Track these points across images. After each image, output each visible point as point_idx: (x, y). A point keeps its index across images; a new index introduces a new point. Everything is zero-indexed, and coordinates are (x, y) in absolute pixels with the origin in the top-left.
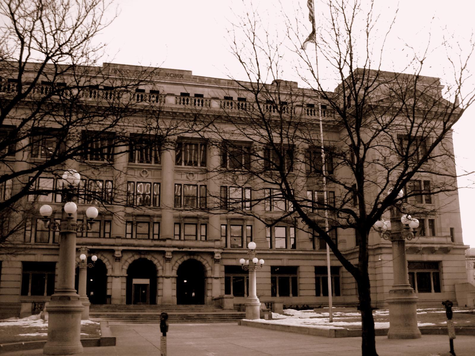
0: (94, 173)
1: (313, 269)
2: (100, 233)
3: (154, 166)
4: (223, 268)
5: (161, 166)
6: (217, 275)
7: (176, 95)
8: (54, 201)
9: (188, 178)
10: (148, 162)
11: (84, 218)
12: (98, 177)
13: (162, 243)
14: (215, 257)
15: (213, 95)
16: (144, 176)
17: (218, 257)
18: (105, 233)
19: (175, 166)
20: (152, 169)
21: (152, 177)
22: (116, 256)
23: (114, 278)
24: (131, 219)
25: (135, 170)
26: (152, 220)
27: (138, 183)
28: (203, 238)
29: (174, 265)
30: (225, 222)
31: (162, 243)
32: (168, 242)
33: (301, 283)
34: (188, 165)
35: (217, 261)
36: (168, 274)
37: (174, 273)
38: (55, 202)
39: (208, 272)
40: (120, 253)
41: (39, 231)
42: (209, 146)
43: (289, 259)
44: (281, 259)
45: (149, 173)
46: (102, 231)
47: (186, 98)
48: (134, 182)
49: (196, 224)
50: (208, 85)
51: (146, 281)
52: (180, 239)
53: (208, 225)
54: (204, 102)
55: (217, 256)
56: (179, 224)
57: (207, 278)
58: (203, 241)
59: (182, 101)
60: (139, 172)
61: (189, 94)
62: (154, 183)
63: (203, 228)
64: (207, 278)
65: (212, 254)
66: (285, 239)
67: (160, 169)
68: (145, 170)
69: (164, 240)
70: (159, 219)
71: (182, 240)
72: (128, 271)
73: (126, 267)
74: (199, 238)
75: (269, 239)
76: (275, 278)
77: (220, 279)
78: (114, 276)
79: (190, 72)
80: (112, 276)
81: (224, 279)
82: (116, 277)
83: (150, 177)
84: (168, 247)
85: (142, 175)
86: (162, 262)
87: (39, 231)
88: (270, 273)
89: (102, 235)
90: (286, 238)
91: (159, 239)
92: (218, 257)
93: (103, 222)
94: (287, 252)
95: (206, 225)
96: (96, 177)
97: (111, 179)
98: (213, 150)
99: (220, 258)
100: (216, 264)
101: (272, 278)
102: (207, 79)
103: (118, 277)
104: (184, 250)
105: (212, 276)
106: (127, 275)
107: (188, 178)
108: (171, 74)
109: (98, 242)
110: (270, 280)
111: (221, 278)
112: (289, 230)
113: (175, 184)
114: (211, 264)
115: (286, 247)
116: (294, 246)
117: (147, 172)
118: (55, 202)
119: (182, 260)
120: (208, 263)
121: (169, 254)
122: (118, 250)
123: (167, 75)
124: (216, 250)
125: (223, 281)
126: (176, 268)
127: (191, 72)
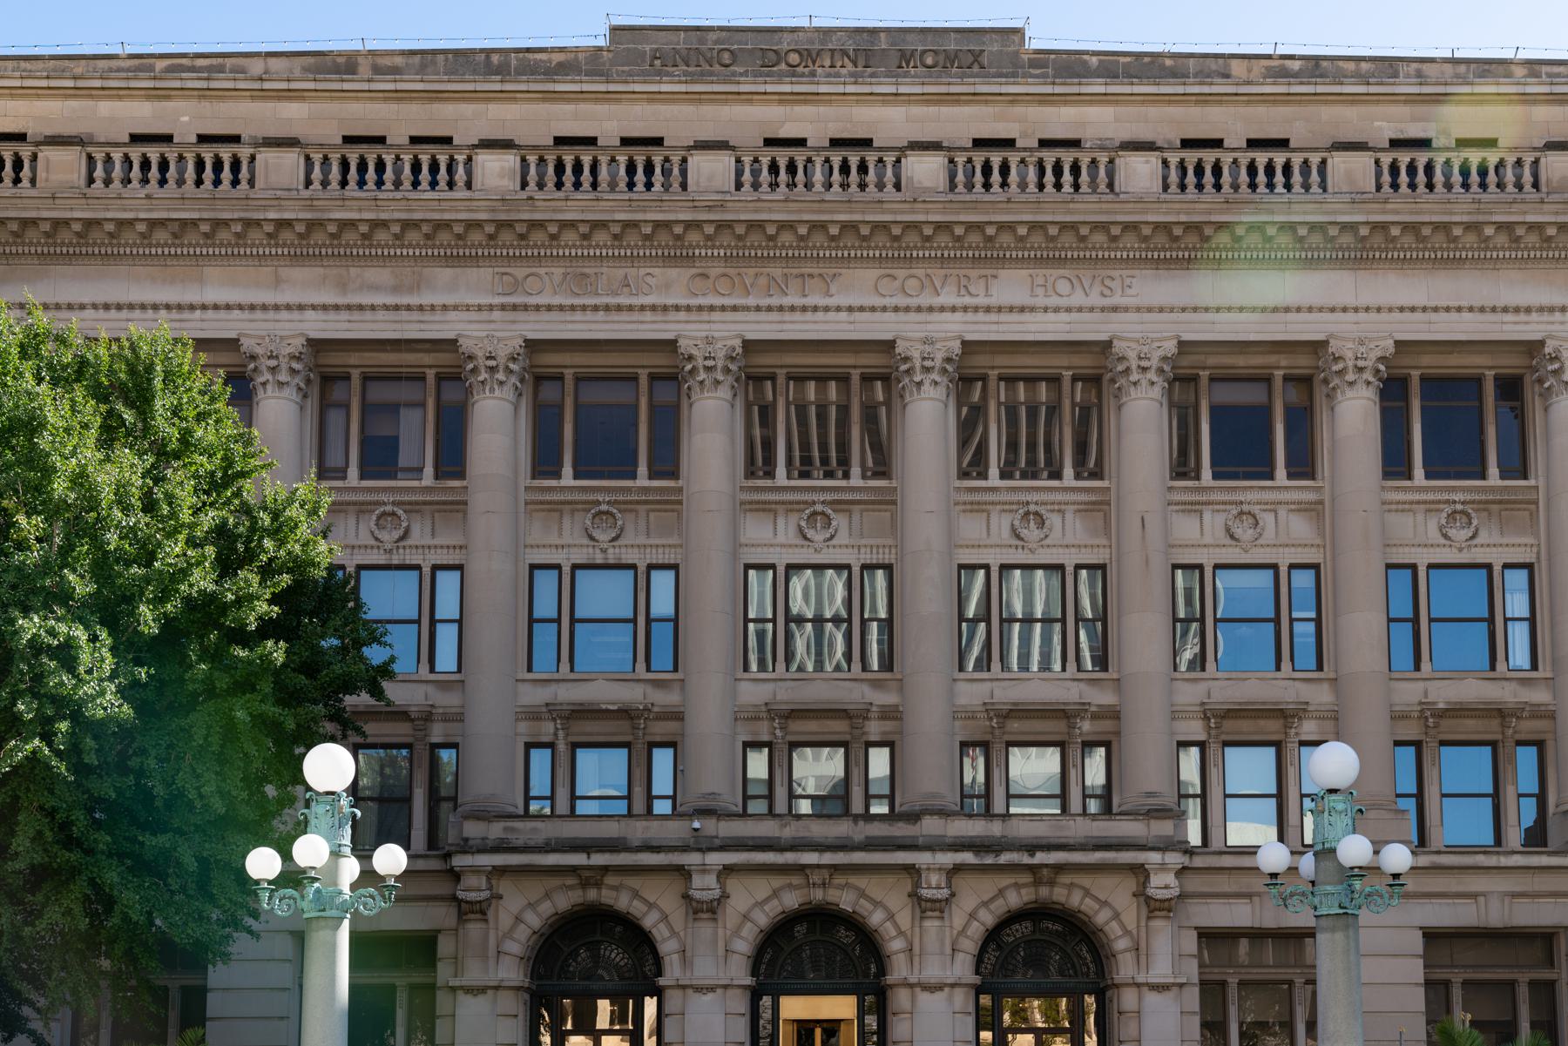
0: (596, 534)
1: (1417, 942)
2: (629, 797)
3: (571, 489)
4: (1190, 943)
5: (680, 490)
6: (1161, 970)
7: (949, 149)
8: (424, 667)
9: (1018, 537)
10: (829, 475)
11: (556, 734)
12: (611, 551)
13: (901, 830)
14: (1151, 892)
15: (1126, 134)
16: (818, 536)
17: (1166, 887)
18: (650, 798)
19: (958, 483)
20: (425, 503)
21: (853, 542)
22: (697, 895)
23: (461, 996)
24: (547, 730)
25: (775, 513)
26: (857, 732)
27: (793, 568)
28: (1093, 805)
29: (963, 932)
30: (1195, 730)
31: (901, 830)
32: (931, 826)
33: (510, 1022)
34: (1024, 476)
35: (1156, 908)
36: (933, 970)
37: (963, 969)
38: (432, 670)
39: (1120, 957)
40: (711, 880)
41: (1194, 796)
42: (1113, 381)
43: (1514, 895)
44: (1474, 896)
45: (839, 521)
46: (639, 791)
47: (996, 159)
48: (987, 567)
49: (1277, 745)
50: (1101, 89)
51: (841, 1007)
52: (771, 813)
53: (1115, 747)
54: (1013, 171)
55: (1163, 883)
56: (985, 746)
57: (1117, 986)
58: (1094, 817)
59: (836, 176)
60: (794, 518)
61: (661, 139)
62: (1078, 567)
63: (1526, 758)
64: (1117, 986)
65: (1140, 871)
66: (1273, 801)
67: (889, 502)
68: (819, 508)
69: (914, 817)
70: (889, 726)
71: (970, 816)
72: (757, 962)
73: (744, 946)
74: (1075, 805)
75: (1411, 804)
76: (1447, 984)
77: (1175, 989)
78: (691, 986)
79: (1016, 38)
80: (684, 987)
81: (1196, 990)
82: (699, 989)
83: (842, 538)
84: (930, 847)
85: (810, 533)
86: (904, 919)
87: (1194, 796)
88: (211, 983)
89: (639, 807)
90: (1496, 796)
91: (892, 817)
92: (1166, 887)
93: (640, 747)
94: (1504, 861)
95: (1540, 745)
96: (604, 551)
97: (885, 557)
98: (1350, 393)
99: (1175, 892)
100: (1157, 924)
101: (1429, 984)
102: (1094, 59)
103: (712, 989)
104: (1005, 858)
105: (1141, 979)
106: (749, 981)
107: (1018, 537)
108: (924, 52)
109: (615, 835)
110: (1421, 992)
111: (1181, 985)
112: (1513, 760)
113: (1175, 567)
114: (678, 926)
115: (1498, 841)
116: (1537, 837)
117: (1041, 522)
118: (432, 670)
119: (546, 908)
120: (891, 917)
121: (934, 879)
122: (476, 870)
123: (906, 57)
124: (1154, 857)
125: (1193, 998)
126: (970, 946)
127: (1018, 32)
